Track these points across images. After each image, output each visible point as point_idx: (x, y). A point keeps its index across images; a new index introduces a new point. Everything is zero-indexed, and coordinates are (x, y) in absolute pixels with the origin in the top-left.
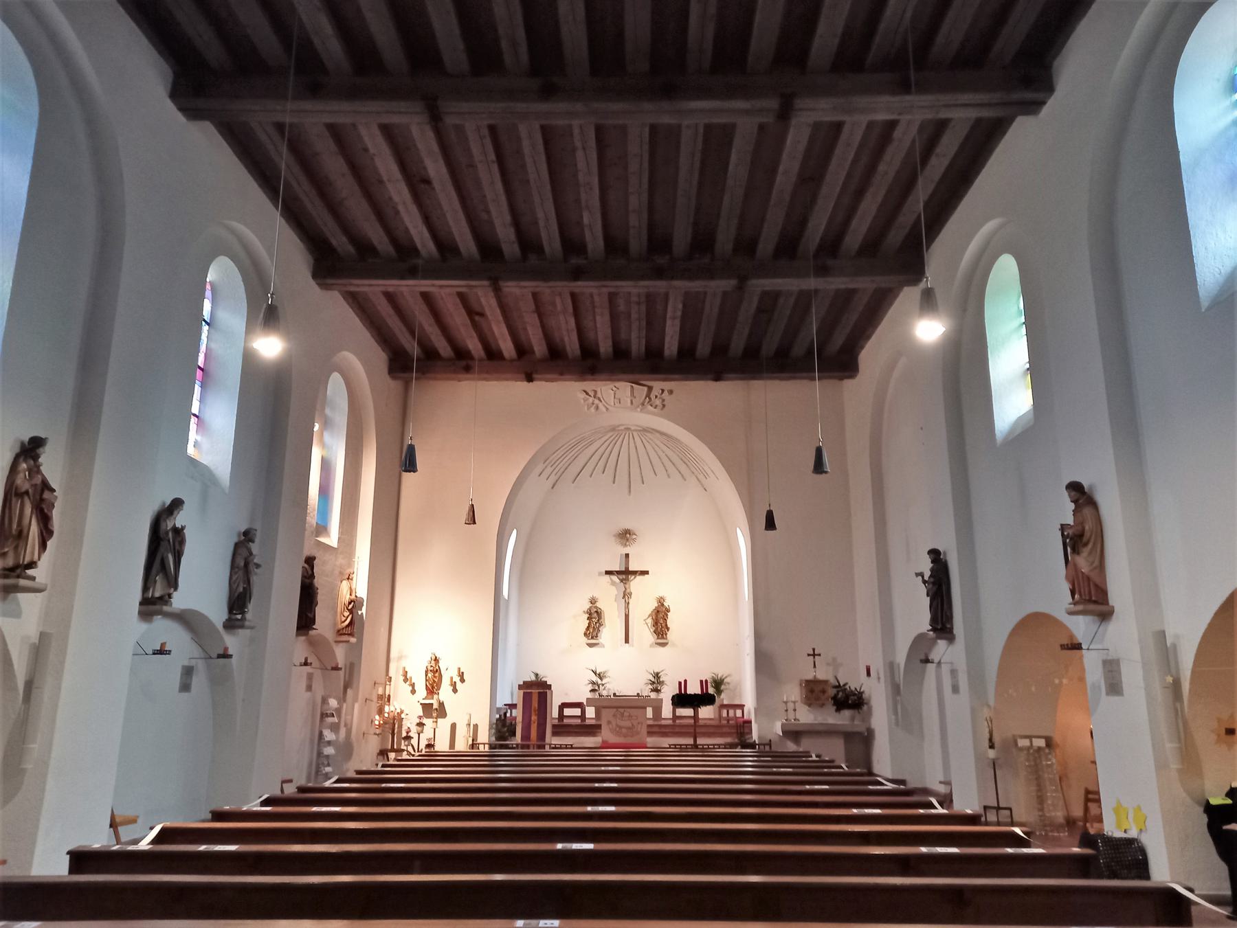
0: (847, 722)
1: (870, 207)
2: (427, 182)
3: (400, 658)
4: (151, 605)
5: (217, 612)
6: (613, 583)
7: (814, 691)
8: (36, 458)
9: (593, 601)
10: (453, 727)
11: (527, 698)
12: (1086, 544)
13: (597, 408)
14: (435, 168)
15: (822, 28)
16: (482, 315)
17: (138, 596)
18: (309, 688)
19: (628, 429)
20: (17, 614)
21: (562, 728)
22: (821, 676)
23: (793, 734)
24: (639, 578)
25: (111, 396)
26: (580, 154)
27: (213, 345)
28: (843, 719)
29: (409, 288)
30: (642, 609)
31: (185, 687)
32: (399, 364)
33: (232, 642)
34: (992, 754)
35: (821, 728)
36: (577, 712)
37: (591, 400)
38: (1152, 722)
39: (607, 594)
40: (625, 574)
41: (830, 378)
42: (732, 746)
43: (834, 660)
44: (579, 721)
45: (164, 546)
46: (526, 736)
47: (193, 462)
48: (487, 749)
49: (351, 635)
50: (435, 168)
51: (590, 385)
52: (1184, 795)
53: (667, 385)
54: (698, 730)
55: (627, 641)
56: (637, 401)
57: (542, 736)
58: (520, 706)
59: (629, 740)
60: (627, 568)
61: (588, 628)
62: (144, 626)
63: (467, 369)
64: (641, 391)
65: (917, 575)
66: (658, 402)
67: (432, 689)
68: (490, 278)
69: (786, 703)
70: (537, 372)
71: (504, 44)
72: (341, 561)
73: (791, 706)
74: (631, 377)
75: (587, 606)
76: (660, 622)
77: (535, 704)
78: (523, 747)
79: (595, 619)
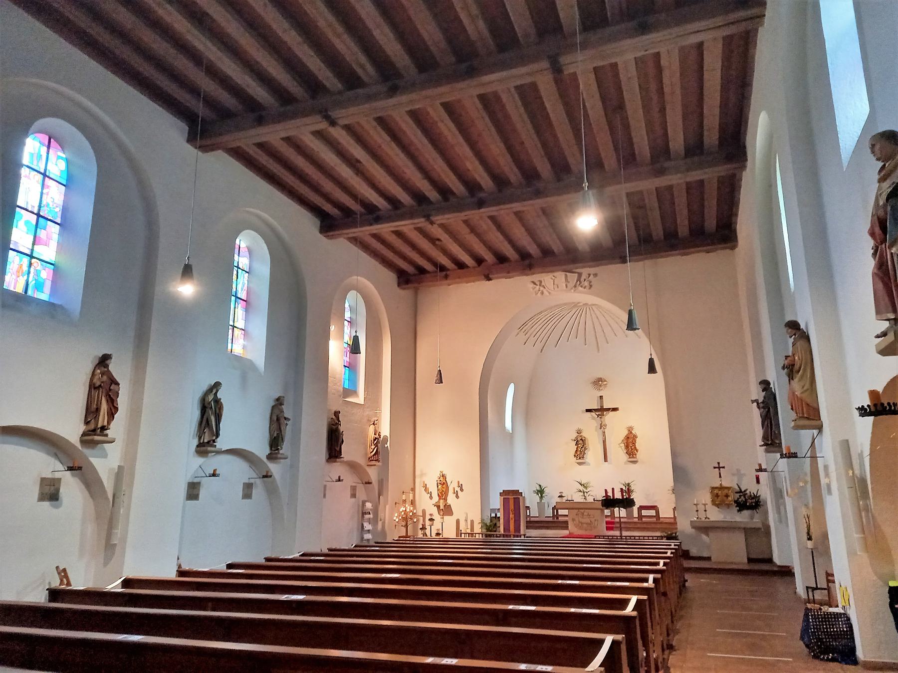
2: (358, 161)
3: (422, 475)
4: (204, 447)
5: (261, 449)
6: (593, 418)
7: (719, 496)
8: (107, 366)
9: (579, 432)
10: (458, 522)
11: (506, 502)
13: (542, 293)
14: (358, 152)
17: (195, 442)
18: (353, 495)
19: (586, 304)
20: (105, 456)
21: (532, 524)
22: (725, 484)
23: (705, 528)
24: (611, 413)
25: (155, 325)
27: (252, 285)
28: (743, 518)
29: (385, 229)
31: (247, 495)
32: (404, 279)
33: (274, 468)
34: (810, 544)
35: (725, 525)
36: (652, 513)
38: (844, 516)
39: (589, 427)
40: (601, 411)
41: (699, 252)
42: (662, 537)
43: (738, 471)
45: (210, 411)
47: (238, 358)
50: (358, 152)
51: (536, 277)
52: (875, 578)
53: (592, 270)
55: (606, 460)
57: (517, 529)
58: (502, 510)
59: (588, 533)
60: (602, 407)
62: (200, 460)
63: (446, 277)
64: (573, 277)
65: (753, 402)
66: (586, 284)
67: (443, 495)
68: (424, 217)
69: (696, 505)
71: (354, 66)
72: (367, 412)
73: (701, 508)
74: (564, 267)
75: (626, 432)
76: (630, 444)
77: (512, 507)
78: (504, 536)
79: (581, 446)
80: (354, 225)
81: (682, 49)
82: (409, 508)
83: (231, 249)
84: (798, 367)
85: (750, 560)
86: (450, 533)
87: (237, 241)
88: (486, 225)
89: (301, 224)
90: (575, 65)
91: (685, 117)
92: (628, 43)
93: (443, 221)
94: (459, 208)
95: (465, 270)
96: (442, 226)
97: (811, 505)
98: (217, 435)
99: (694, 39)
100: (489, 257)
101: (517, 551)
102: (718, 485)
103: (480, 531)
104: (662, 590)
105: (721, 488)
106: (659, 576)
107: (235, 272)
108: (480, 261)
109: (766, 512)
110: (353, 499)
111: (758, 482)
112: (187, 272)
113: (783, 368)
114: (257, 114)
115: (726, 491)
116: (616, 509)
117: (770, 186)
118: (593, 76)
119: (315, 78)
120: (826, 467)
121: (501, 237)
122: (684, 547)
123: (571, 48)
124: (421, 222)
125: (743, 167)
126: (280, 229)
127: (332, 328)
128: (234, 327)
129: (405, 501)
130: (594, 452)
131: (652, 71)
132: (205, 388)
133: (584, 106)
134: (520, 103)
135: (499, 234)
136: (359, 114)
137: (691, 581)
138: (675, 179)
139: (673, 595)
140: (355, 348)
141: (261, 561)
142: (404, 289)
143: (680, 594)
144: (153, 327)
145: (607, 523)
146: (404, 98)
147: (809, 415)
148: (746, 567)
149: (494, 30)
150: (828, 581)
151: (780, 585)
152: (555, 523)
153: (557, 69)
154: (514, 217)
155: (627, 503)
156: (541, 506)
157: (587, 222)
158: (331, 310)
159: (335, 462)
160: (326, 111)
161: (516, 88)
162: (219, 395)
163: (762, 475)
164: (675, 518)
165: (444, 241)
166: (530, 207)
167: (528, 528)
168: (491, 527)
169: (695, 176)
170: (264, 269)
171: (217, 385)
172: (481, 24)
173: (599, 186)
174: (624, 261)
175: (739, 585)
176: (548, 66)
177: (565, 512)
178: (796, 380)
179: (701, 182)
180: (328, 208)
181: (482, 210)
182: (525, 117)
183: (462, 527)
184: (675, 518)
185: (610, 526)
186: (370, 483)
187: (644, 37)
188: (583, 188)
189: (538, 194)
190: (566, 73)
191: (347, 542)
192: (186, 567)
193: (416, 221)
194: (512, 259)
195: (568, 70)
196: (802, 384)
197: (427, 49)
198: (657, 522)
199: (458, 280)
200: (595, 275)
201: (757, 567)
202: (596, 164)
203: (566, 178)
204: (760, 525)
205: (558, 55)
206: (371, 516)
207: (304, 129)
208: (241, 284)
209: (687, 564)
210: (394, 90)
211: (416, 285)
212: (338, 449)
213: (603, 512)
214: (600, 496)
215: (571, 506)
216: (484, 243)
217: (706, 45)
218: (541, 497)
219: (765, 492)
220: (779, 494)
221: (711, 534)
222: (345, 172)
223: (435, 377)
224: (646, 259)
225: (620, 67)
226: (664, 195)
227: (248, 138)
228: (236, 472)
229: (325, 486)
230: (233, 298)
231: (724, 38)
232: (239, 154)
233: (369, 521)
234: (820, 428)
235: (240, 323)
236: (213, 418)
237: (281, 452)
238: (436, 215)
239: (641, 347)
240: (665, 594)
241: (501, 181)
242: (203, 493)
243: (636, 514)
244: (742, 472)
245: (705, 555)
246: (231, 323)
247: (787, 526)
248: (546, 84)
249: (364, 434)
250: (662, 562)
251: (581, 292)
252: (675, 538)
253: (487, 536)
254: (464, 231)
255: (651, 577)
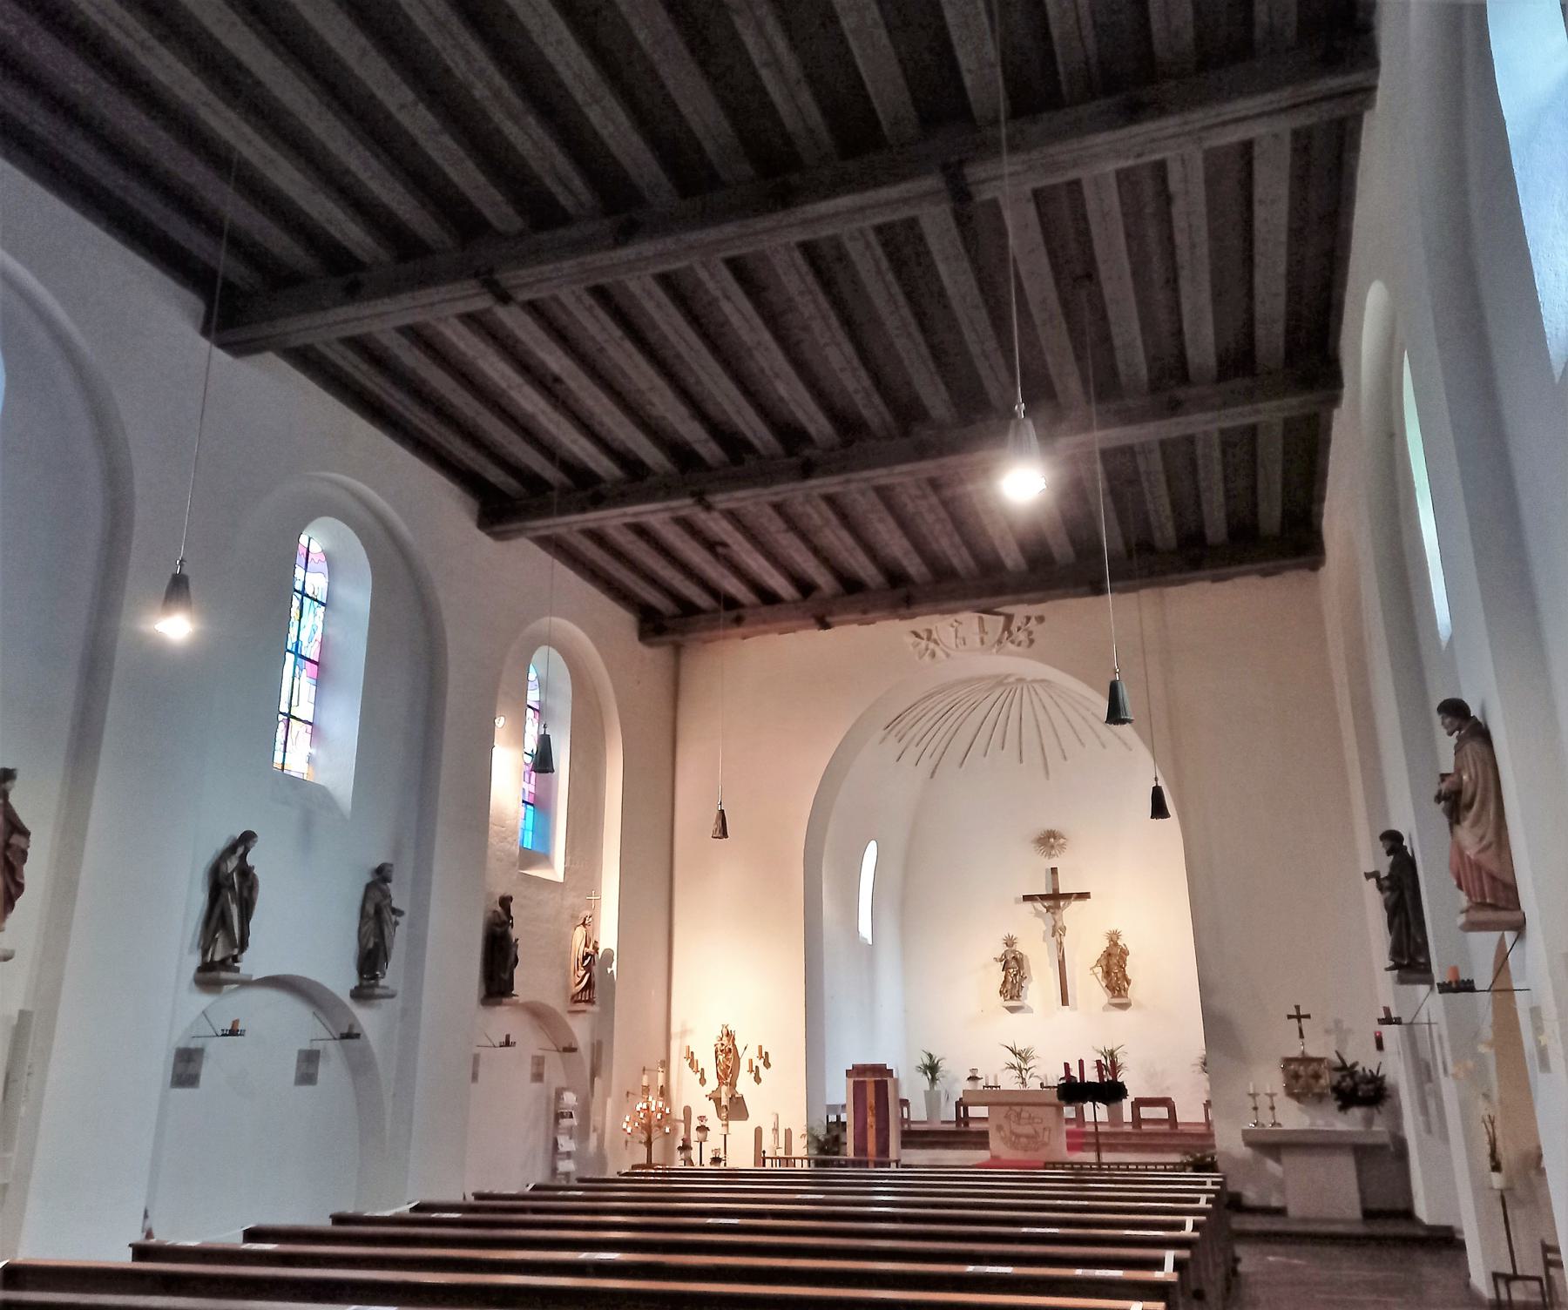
0: (1359, 1128)
1: (1197, 299)
2: (557, 379)
3: (684, 1033)
5: (340, 977)
6: (1038, 914)
7: (1302, 1078)
9: (1010, 942)
10: (758, 1132)
11: (858, 1090)
12: (1470, 806)
13: (933, 655)
14: (555, 360)
15: (965, 59)
16: (725, 545)
17: (195, 960)
18: (538, 1077)
19: (1020, 680)
21: (915, 1138)
23: (1271, 1146)
24: (1075, 905)
26: (727, 307)
27: (330, 631)
28: (1349, 1123)
29: (612, 519)
30: (1085, 952)
32: (652, 625)
33: (367, 1018)
34: (1497, 1180)
35: (1311, 1139)
36: (1162, 1113)
37: (923, 643)
40: (1055, 899)
42: (1183, 1166)
43: (1338, 1022)
44: (1165, 1127)
45: (230, 893)
46: (861, 1148)
47: (296, 783)
48: (805, 1167)
49: (590, 1001)
50: (555, 360)
51: (920, 623)
53: (1035, 610)
54: (1102, 1140)
55: (1065, 1002)
56: (991, 638)
57: (883, 1149)
58: (850, 1108)
60: (1056, 890)
61: (1005, 982)
62: (205, 1000)
63: (738, 621)
64: (995, 623)
66: (1022, 636)
67: (728, 1074)
68: (693, 495)
69: (1254, 1096)
70: (831, 613)
71: (549, 181)
72: (571, 899)
73: (1264, 1102)
74: (976, 602)
76: (1114, 969)
78: (854, 1163)
79: (1014, 970)
80: (544, 511)
81: (1211, 156)
82: (655, 1103)
83: (286, 558)
84: (1468, 798)
85: (1369, 1215)
86: (741, 1158)
87: (303, 540)
88: (819, 517)
89: (437, 509)
90: (998, 183)
91: (1217, 296)
92: (1101, 140)
93: (732, 505)
94: (765, 475)
95: (777, 607)
96: (733, 516)
97: (1495, 1095)
98: (243, 945)
99: (1234, 136)
100: (823, 579)
101: (883, 1200)
102: (1296, 1053)
103: (803, 1153)
104: (1193, 1286)
105: (1305, 1060)
106: (1185, 1254)
107: (296, 603)
108: (805, 587)
109: (1397, 1114)
110: (536, 1085)
111: (1380, 1045)
112: (177, 589)
113: (1439, 798)
114: (344, 274)
115: (1314, 1066)
116: (1088, 1106)
117: (1391, 435)
118: (1032, 207)
119: (464, 201)
120: (1535, 1012)
121: (849, 540)
122: (1233, 1187)
123: (988, 149)
124: (685, 506)
125: (1335, 401)
126: (403, 528)
127: (500, 722)
128: (289, 716)
129: (646, 1090)
130: (1040, 986)
131: (1148, 188)
132: (221, 843)
133: (1017, 276)
134: (885, 264)
135: (845, 535)
136: (562, 281)
137: (1250, 1260)
138: (1204, 424)
139: (1213, 1293)
140: (543, 762)
141: (324, 1223)
142: (651, 645)
143: (1228, 1289)
144: (110, 716)
145: (1069, 1134)
146: (647, 248)
147: (1496, 900)
148: (1360, 1229)
149: (831, 112)
150: (1548, 1264)
151: (1429, 1269)
152: (962, 1135)
153: (961, 195)
154: (872, 495)
155: (1110, 1091)
156: (932, 1100)
157: (1022, 484)
158: (497, 688)
159: (500, 1004)
160: (491, 271)
161: (879, 229)
162: (250, 860)
163: (1391, 1033)
164: (1208, 1123)
165: (735, 547)
166: (903, 476)
167: (904, 1145)
168: (827, 1144)
169: (1237, 417)
170: (358, 598)
171: (247, 838)
172: (806, 97)
173: (1047, 436)
174: (1097, 589)
175: (1350, 1268)
176: (942, 185)
177: (982, 1111)
178: (1466, 824)
179: (1253, 430)
180: (495, 475)
181: (813, 482)
182: (896, 289)
183: (768, 1144)
184: (1208, 1123)
185: (1077, 1140)
186: (573, 1050)
187: (1135, 129)
188: (1014, 415)
189: (922, 452)
190: (978, 199)
191: (515, 1176)
192: (165, 1236)
193: (674, 504)
194: (872, 585)
195: (985, 194)
196: (1480, 832)
197: (699, 149)
198: (1171, 1134)
199: (762, 627)
200: (1041, 619)
201: (1379, 1228)
202: (1040, 392)
203: (977, 418)
204: (1385, 1139)
205: (961, 163)
206: (575, 1122)
207: (445, 309)
208: (308, 628)
209: (1240, 1222)
210: (626, 233)
211: (677, 638)
212: (506, 976)
213: (1059, 1109)
214: (1055, 1076)
215: (996, 1098)
216: (816, 551)
217: (1257, 150)
218: (933, 1080)
219: (1395, 1069)
220: (1424, 1072)
221: (1285, 1158)
222: (529, 401)
223: (712, 824)
224: (1142, 587)
225: (1088, 192)
226: (1180, 456)
227: (328, 327)
228: (283, 1026)
229: (476, 1059)
230: (290, 657)
231: (1296, 134)
232: (308, 361)
233: (570, 1132)
234: (1519, 928)
235: (304, 710)
236: (235, 910)
237: (382, 982)
238: (716, 491)
239: (1135, 766)
240: (1199, 1295)
241: (848, 425)
242: (207, 1072)
243: (1127, 1115)
244: (1345, 1025)
245: (1275, 1202)
246: (284, 708)
247: (1445, 1138)
248: (937, 224)
249: (564, 942)
250: (1189, 1221)
251: (1010, 654)
252: (1212, 1167)
253: (819, 1163)
254: (774, 527)
255: (1169, 1256)
